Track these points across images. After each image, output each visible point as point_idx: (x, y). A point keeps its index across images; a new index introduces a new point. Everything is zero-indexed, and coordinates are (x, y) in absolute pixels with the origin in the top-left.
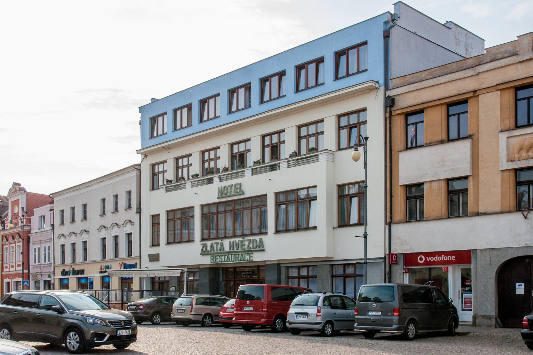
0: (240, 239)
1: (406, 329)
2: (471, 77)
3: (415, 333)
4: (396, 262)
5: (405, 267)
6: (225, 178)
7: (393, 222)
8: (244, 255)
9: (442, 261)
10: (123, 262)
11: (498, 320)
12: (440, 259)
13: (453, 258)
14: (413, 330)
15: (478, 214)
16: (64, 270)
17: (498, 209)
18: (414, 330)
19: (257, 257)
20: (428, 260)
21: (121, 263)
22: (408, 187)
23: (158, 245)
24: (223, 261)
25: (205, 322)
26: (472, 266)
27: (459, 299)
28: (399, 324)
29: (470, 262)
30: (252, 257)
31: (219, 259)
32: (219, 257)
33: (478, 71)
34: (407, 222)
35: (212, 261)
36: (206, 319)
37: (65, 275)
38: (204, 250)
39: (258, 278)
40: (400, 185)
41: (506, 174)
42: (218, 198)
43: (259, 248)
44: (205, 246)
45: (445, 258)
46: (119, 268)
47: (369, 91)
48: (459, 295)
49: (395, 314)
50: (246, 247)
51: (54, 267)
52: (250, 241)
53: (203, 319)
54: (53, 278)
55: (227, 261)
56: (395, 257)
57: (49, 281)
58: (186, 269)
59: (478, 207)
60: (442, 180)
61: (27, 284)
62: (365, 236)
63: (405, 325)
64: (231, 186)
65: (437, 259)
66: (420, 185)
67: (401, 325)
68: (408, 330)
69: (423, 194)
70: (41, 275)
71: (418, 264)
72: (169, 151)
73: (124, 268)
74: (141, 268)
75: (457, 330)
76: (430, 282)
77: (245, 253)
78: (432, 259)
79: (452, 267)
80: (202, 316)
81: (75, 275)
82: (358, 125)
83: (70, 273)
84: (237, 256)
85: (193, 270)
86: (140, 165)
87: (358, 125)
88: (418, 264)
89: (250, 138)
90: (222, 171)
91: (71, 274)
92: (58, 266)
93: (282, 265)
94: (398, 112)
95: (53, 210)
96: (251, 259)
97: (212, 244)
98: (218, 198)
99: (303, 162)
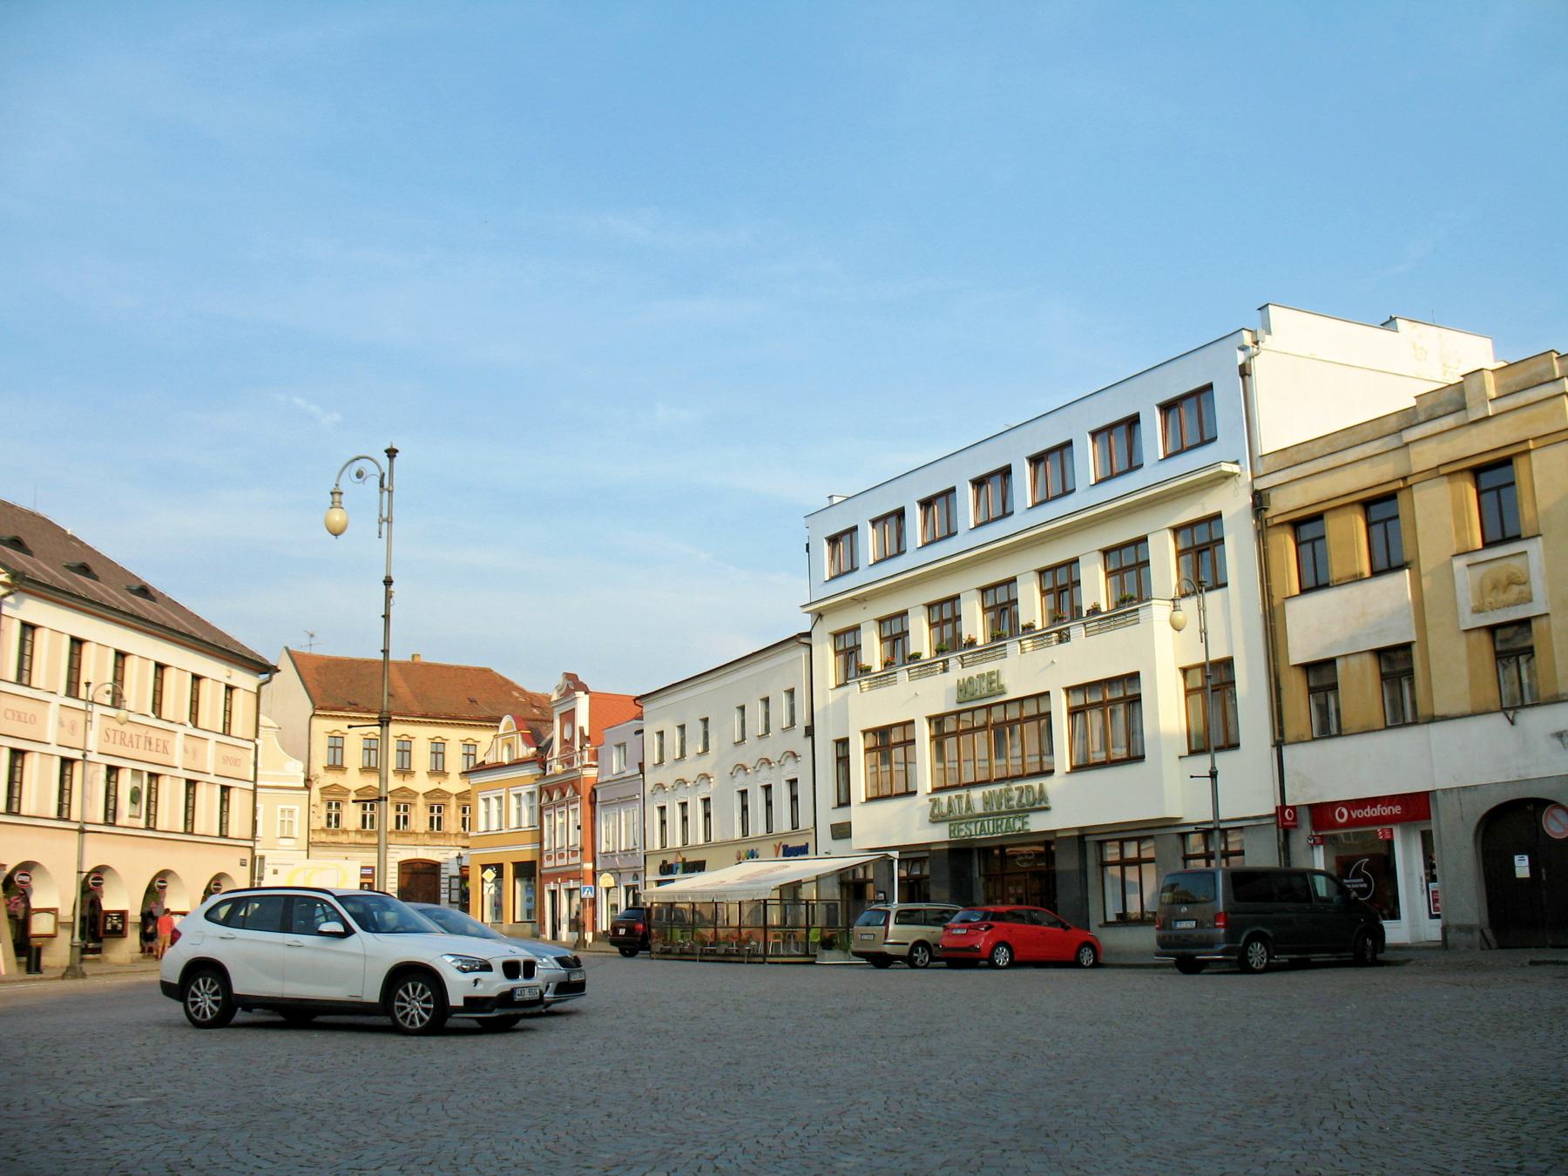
0: (1003, 786)
2: (1455, 431)
3: (1268, 960)
4: (1295, 824)
5: (1314, 834)
6: (1097, 628)
11: (1489, 933)
12: (1374, 812)
13: (1397, 810)
14: (1263, 953)
15: (1433, 719)
16: (664, 862)
18: (1265, 954)
19: (1037, 823)
20: (1354, 816)
22: (1308, 668)
23: (848, 803)
24: (974, 833)
25: (916, 958)
27: (1423, 892)
28: (1227, 943)
29: (1429, 817)
30: (1027, 823)
31: (965, 830)
34: (1387, 728)
35: (953, 835)
36: (917, 952)
38: (936, 812)
39: (1047, 866)
40: (1295, 666)
41: (1473, 636)
42: (959, 702)
43: (1040, 803)
44: (935, 803)
45: (1384, 811)
46: (774, 854)
47: (1224, 480)
48: (1422, 886)
50: (1014, 803)
52: (1020, 789)
56: (1289, 813)
62: (1213, 775)
63: (1241, 945)
64: (981, 677)
65: (1369, 812)
66: (1330, 663)
69: (1333, 681)
70: (620, 874)
71: (1335, 825)
73: (784, 855)
74: (816, 854)
75: (1380, 956)
76: (1361, 864)
78: (1360, 813)
81: (687, 872)
82: (1211, 546)
83: (677, 868)
84: (999, 822)
85: (913, 855)
86: (809, 635)
88: (1335, 825)
90: (1088, 614)
91: (680, 871)
92: (654, 853)
93: (1087, 839)
94: (1276, 521)
95: (642, 731)
96: (1027, 827)
98: (959, 702)
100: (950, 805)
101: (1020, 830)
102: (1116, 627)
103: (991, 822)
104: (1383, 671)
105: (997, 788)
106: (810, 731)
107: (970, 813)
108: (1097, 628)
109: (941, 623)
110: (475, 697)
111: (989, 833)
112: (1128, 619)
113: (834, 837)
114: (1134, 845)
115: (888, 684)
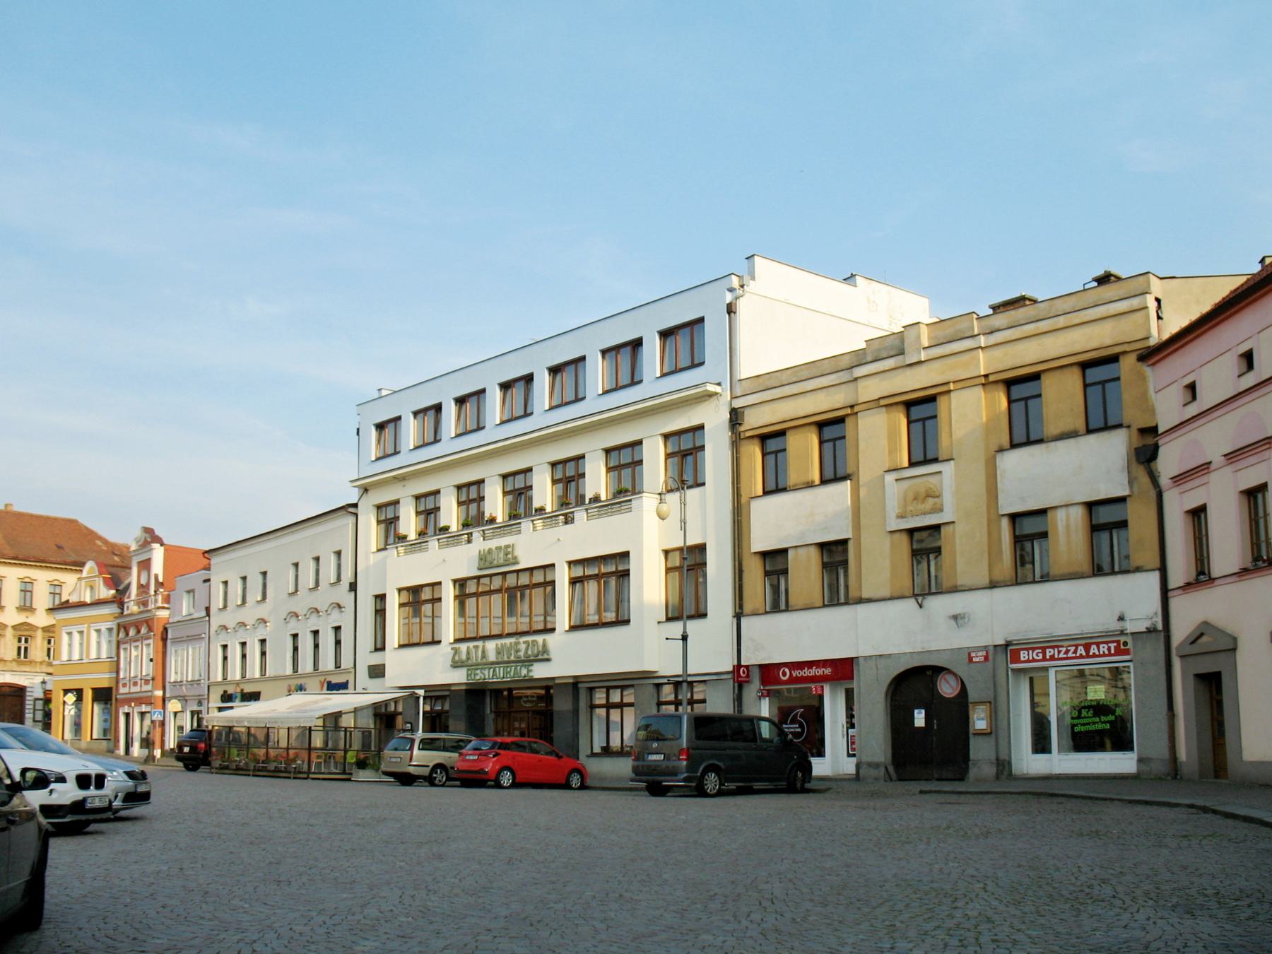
0: (512, 640)
1: (701, 781)
4: (747, 679)
5: (762, 688)
7: (745, 613)
8: (519, 667)
9: (820, 675)
10: (325, 679)
11: (891, 769)
12: (810, 673)
13: (828, 671)
14: (716, 781)
15: (860, 601)
17: (887, 593)
18: (718, 782)
19: (540, 671)
20: (794, 675)
21: (322, 680)
22: (765, 555)
24: (487, 677)
25: (435, 778)
26: (855, 685)
27: (843, 737)
31: (480, 674)
32: (481, 672)
33: (855, 376)
34: (824, 606)
36: (436, 773)
37: (227, 702)
38: (457, 658)
40: (755, 553)
41: (897, 536)
42: (480, 569)
44: (456, 651)
45: (818, 672)
47: (708, 398)
48: (843, 731)
49: (681, 757)
50: (521, 654)
51: (209, 686)
53: (431, 773)
54: (206, 706)
55: (493, 678)
56: (743, 670)
57: (199, 712)
58: (421, 692)
59: (861, 591)
60: (811, 544)
61: (159, 716)
62: (684, 638)
63: (699, 774)
64: (499, 548)
65: (806, 672)
67: (692, 775)
68: (705, 782)
72: (403, 484)
73: (328, 689)
74: (355, 689)
77: (520, 664)
78: (799, 673)
79: (830, 686)
80: (428, 770)
82: (694, 452)
85: (436, 693)
87: (576, 478)
89: (399, 499)
90: (590, 502)
92: (217, 684)
93: (580, 685)
94: (748, 434)
96: (531, 674)
97: (468, 647)
99: (609, 510)
100: (468, 653)
102: (613, 513)
105: (508, 641)
106: (353, 587)
107: (484, 660)
108: (597, 513)
109: (478, 500)
112: (622, 508)
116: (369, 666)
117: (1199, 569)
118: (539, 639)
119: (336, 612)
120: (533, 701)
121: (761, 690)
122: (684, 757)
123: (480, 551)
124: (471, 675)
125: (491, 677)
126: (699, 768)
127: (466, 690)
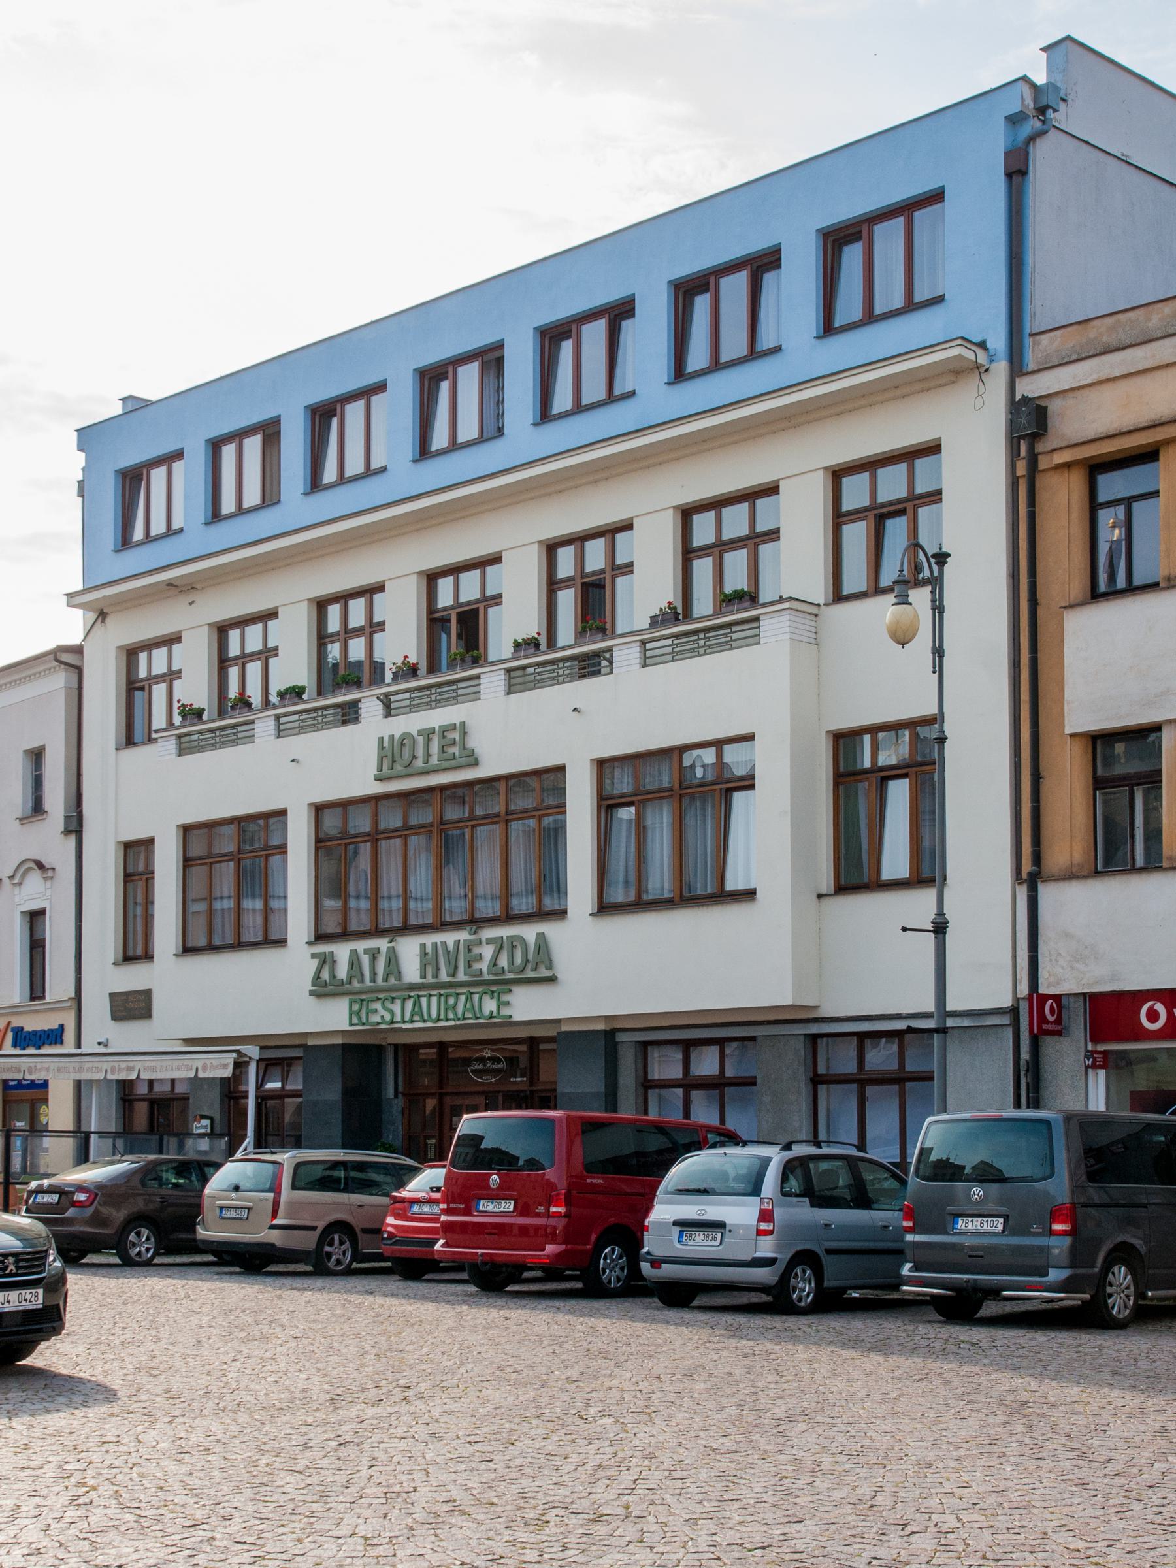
0: (463, 936)
4: (1058, 1027)
10: (9, 1023)
14: (1127, 1288)
18: (1132, 1288)
24: (398, 1018)
31: (382, 1012)
34: (1097, 873)
35: (355, 1021)
36: (331, 1244)
38: (325, 975)
40: (1072, 736)
42: (379, 779)
44: (326, 961)
50: (484, 966)
52: (499, 944)
56: (1051, 1006)
58: (253, 1052)
62: (940, 928)
63: (1096, 1270)
64: (428, 734)
68: (1109, 1290)
73: (15, 1045)
74: (79, 1046)
84: (451, 1001)
94: (1059, 458)
96: (505, 1011)
97: (354, 953)
100: (352, 965)
101: (491, 1017)
102: (709, 650)
103: (434, 1000)
104: (1099, 772)
105: (450, 938)
106: (75, 826)
107: (392, 981)
108: (669, 649)
109: (343, 635)
110: (379, 1481)
111: (430, 1019)
112: (734, 636)
113: (116, 1017)
114: (712, 1053)
115: (235, 742)
116: (111, 995)
117: (140, 886)
118: (529, 932)
119: (35, 878)
120: (499, 1071)
121: (1091, 1052)
122: (562, 1210)
123: (381, 740)
124: (358, 1013)
125: (407, 1018)
126: (1096, 1254)
127: (343, 1045)
